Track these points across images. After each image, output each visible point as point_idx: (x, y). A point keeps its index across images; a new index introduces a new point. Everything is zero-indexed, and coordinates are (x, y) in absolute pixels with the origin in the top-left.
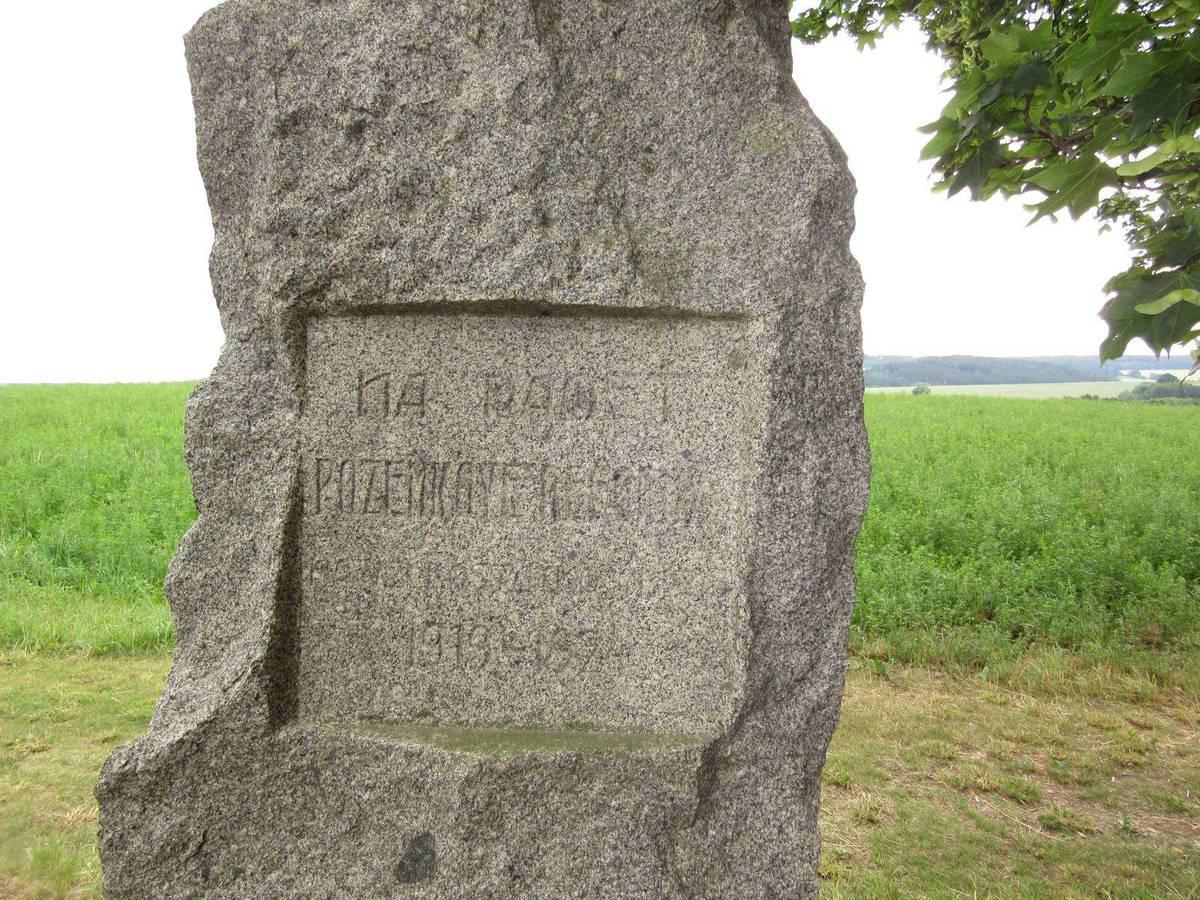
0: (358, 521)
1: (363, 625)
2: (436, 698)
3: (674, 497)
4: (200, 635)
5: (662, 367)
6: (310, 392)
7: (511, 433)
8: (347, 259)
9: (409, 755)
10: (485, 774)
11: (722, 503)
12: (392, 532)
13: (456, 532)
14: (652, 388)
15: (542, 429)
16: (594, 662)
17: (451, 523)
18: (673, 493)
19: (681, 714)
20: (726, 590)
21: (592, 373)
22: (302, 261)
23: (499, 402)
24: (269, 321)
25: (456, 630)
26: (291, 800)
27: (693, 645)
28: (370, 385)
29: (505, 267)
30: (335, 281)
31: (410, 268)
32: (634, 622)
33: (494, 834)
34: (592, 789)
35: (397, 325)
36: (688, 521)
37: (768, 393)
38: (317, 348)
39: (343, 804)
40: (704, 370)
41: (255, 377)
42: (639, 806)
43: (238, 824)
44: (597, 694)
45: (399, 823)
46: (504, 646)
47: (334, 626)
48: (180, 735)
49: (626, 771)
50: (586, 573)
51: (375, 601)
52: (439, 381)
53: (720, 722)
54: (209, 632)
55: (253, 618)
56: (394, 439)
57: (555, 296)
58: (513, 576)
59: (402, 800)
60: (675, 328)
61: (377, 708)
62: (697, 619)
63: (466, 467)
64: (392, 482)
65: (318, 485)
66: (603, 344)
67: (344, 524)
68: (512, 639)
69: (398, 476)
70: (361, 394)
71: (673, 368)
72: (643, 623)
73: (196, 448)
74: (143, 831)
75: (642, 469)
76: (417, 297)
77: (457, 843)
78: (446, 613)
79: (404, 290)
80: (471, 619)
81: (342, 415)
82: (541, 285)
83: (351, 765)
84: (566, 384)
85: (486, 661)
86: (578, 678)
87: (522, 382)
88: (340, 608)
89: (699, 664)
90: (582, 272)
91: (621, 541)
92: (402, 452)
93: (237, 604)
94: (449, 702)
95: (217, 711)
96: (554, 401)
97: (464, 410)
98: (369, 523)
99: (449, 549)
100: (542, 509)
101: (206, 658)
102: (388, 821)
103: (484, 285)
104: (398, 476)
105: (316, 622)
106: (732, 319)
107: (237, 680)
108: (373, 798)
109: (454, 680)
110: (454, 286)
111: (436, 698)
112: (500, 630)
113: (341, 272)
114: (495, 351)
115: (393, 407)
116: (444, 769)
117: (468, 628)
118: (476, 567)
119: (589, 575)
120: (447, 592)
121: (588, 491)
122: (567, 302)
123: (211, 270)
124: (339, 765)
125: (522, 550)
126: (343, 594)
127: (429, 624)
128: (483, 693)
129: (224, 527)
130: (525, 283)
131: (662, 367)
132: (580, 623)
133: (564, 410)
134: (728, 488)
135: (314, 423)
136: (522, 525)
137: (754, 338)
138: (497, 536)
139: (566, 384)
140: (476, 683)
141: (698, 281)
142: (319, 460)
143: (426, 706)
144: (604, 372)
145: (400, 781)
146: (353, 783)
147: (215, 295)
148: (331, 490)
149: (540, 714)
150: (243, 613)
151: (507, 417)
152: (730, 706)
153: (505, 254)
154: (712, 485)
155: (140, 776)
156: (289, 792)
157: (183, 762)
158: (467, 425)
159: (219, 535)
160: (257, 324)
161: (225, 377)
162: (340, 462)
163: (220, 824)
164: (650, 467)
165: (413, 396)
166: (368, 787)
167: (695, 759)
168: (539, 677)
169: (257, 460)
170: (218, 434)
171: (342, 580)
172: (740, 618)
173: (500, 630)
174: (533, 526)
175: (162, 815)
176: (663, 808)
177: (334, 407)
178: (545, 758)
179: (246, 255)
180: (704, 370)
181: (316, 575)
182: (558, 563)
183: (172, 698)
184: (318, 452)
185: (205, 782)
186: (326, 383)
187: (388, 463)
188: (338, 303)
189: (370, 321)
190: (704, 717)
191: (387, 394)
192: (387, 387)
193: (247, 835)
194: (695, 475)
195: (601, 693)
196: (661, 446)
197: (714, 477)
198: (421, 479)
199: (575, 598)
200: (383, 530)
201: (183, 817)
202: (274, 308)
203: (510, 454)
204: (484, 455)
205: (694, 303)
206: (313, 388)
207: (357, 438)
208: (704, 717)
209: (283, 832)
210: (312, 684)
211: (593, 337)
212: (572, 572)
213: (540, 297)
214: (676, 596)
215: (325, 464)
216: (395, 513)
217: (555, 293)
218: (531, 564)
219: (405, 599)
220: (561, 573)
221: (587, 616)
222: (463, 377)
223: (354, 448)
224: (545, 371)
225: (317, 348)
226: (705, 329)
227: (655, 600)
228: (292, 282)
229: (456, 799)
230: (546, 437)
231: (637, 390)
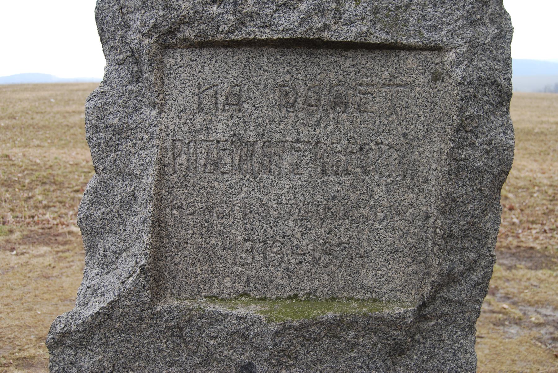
0: (200, 178)
1: (205, 242)
2: (251, 285)
3: (397, 161)
4: (102, 249)
5: (390, 80)
6: (167, 97)
7: (296, 123)
8: (192, 11)
9: (239, 319)
10: (287, 329)
11: (426, 165)
12: (221, 185)
13: (262, 184)
14: (384, 94)
15: (315, 120)
16: (347, 261)
17: (258, 179)
18: (396, 159)
19: (400, 290)
20: (427, 217)
21: (347, 84)
22: (161, 13)
23: (288, 103)
24: (139, 51)
25: (262, 244)
26: (165, 346)
27: (406, 250)
28: (205, 93)
29: (294, 17)
30: (183, 26)
31: (233, 18)
32: (371, 237)
33: (291, 362)
34: (348, 335)
35: (221, 53)
36: (405, 176)
37: (458, 97)
38: (170, 69)
39: (198, 347)
40: (417, 82)
41: (129, 88)
42: (375, 345)
43: (134, 359)
44: (349, 280)
45: (233, 358)
46: (292, 253)
47: (187, 243)
48: (97, 310)
49: (368, 324)
50: (342, 208)
51: (212, 227)
52: (249, 90)
53: (422, 295)
54: (107, 247)
55: (137, 239)
56: (221, 127)
57: (326, 35)
58: (297, 210)
59: (234, 344)
60: (398, 56)
61: (215, 291)
62: (410, 235)
63: (268, 144)
64: (221, 153)
65: (174, 156)
66: (354, 66)
67: (191, 180)
68: (297, 248)
69: (224, 150)
70: (199, 98)
71: (397, 81)
72: (377, 237)
73: (93, 133)
74: (77, 365)
75: (377, 144)
76: (236, 36)
77: (270, 368)
78: (256, 234)
79: (229, 32)
80: (272, 237)
81: (188, 112)
82: (318, 29)
83: (202, 325)
84: (330, 91)
85: (281, 262)
86: (337, 271)
87: (302, 90)
88: (190, 232)
89: (410, 261)
90: (342, 20)
91: (365, 188)
92: (226, 135)
93: (125, 230)
94: (260, 287)
95: (119, 295)
96: (323, 102)
97: (265, 108)
98: (207, 179)
99: (257, 195)
100: (315, 169)
101: (107, 263)
102: (226, 356)
103: (281, 28)
104: (224, 150)
105: (175, 240)
106: (435, 50)
107: (130, 276)
108: (216, 343)
109: (261, 274)
110: (262, 30)
111: (251, 285)
112: (290, 243)
113: (187, 20)
114: (285, 70)
115: (220, 106)
116: (261, 326)
117: (270, 242)
118: (274, 206)
119: (344, 210)
120: (257, 221)
121: (344, 158)
122: (334, 39)
123: (96, 18)
124: (195, 325)
125: (303, 195)
126: (192, 223)
127: (246, 240)
128: (280, 281)
129: (114, 182)
130: (307, 27)
131: (390, 80)
132: (339, 238)
133: (329, 108)
134: (430, 156)
135: (170, 117)
136: (303, 179)
137: (448, 62)
138: (288, 186)
139: (330, 91)
140: (276, 275)
141: (414, 26)
142: (174, 140)
143: (245, 289)
144: (354, 83)
145: (233, 333)
146: (203, 335)
147: (100, 35)
148: (182, 159)
149: (315, 292)
150: (129, 236)
151: (293, 112)
152: (429, 285)
153: (294, 8)
154: (420, 155)
155: (73, 334)
156: (164, 341)
157: (99, 326)
158: (268, 118)
159: (111, 188)
160: (129, 54)
161: (110, 88)
162: (187, 142)
163: (123, 360)
164: (382, 143)
165: (233, 99)
166: (213, 338)
167: (409, 317)
168: (314, 271)
169: (134, 141)
170: (109, 123)
171: (191, 215)
172: (436, 234)
173: (290, 243)
174: (309, 180)
175: (88, 355)
176: (389, 345)
177: (182, 107)
178: (321, 318)
179: (121, 8)
180: (417, 82)
181: (174, 212)
182: (325, 203)
183: (88, 287)
184: (173, 135)
185: (113, 336)
186: (177, 91)
187: (218, 142)
188: (185, 40)
189: (204, 51)
190: (413, 292)
191: (217, 99)
192: (216, 93)
193: (139, 366)
194: (410, 148)
195: (352, 279)
196: (389, 130)
197: (421, 149)
198: (239, 151)
199: (336, 224)
200: (216, 183)
201: (100, 357)
202: (143, 44)
203: (295, 135)
204: (278, 136)
205: (411, 40)
206: (169, 94)
207: (198, 126)
208: (413, 292)
209: (161, 363)
210: (174, 278)
211: (347, 62)
212: (334, 208)
213: (317, 36)
214: (397, 221)
215: (177, 143)
216: (223, 173)
217: (326, 33)
218: (309, 203)
219: (231, 225)
220: (327, 208)
221: (343, 232)
222: (265, 87)
223: (196, 133)
224: (317, 83)
225: (170, 69)
226: (417, 56)
227: (385, 223)
228: (155, 26)
229: (270, 344)
230: (318, 125)
231: (374, 95)
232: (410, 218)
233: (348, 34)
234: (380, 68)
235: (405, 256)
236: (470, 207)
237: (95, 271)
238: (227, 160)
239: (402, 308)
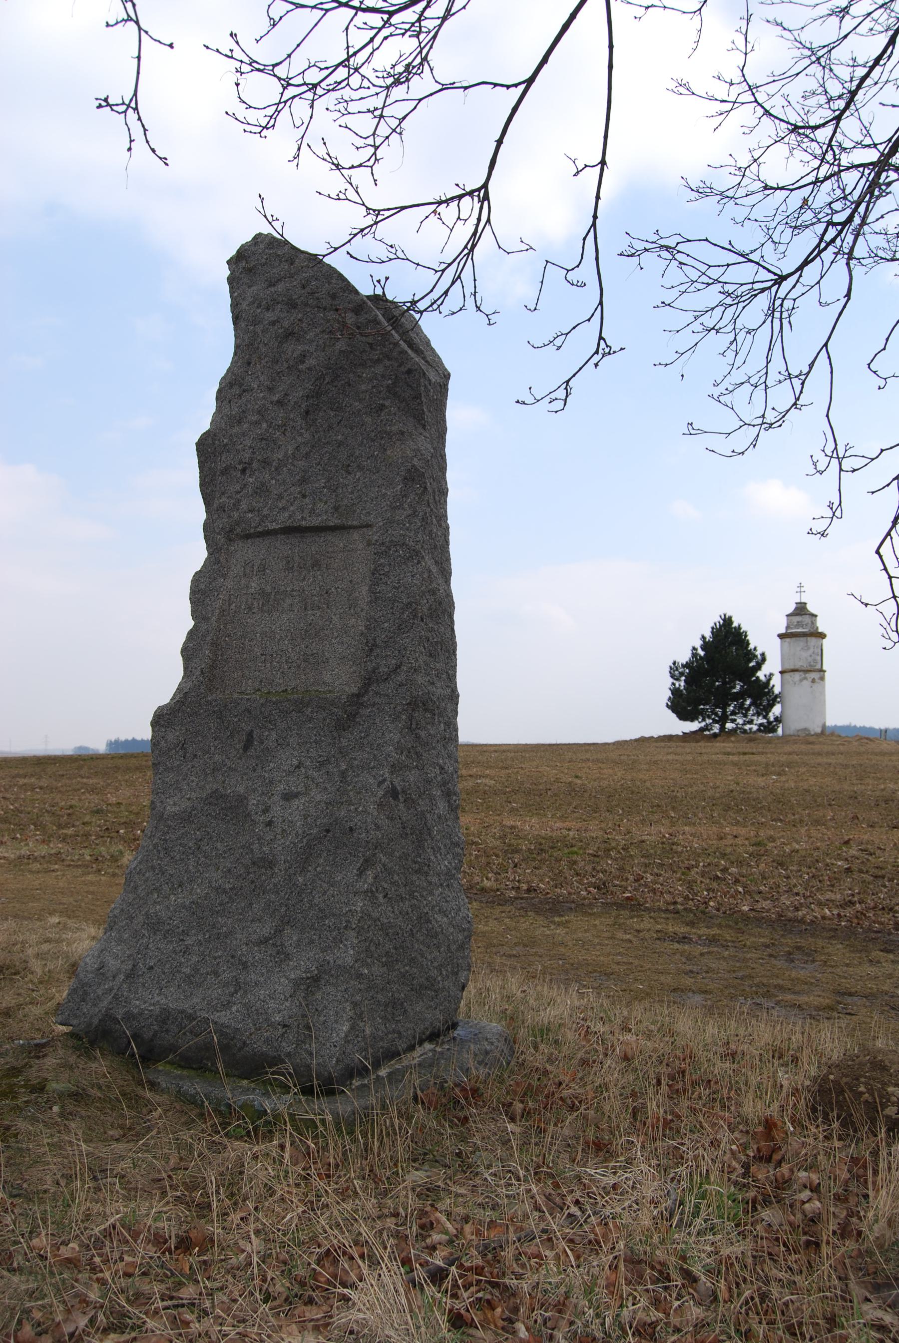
42: (324, 719)
57: (304, 523)
76: (260, 529)
87: (296, 559)
127: (262, 655)
148: (233, 606)
230: (304, 579)
232: (352, 635)
233: (316, 522)
234: (338, 541)
235: (349, 660)
236: (386, 625)
238: (256, 604)
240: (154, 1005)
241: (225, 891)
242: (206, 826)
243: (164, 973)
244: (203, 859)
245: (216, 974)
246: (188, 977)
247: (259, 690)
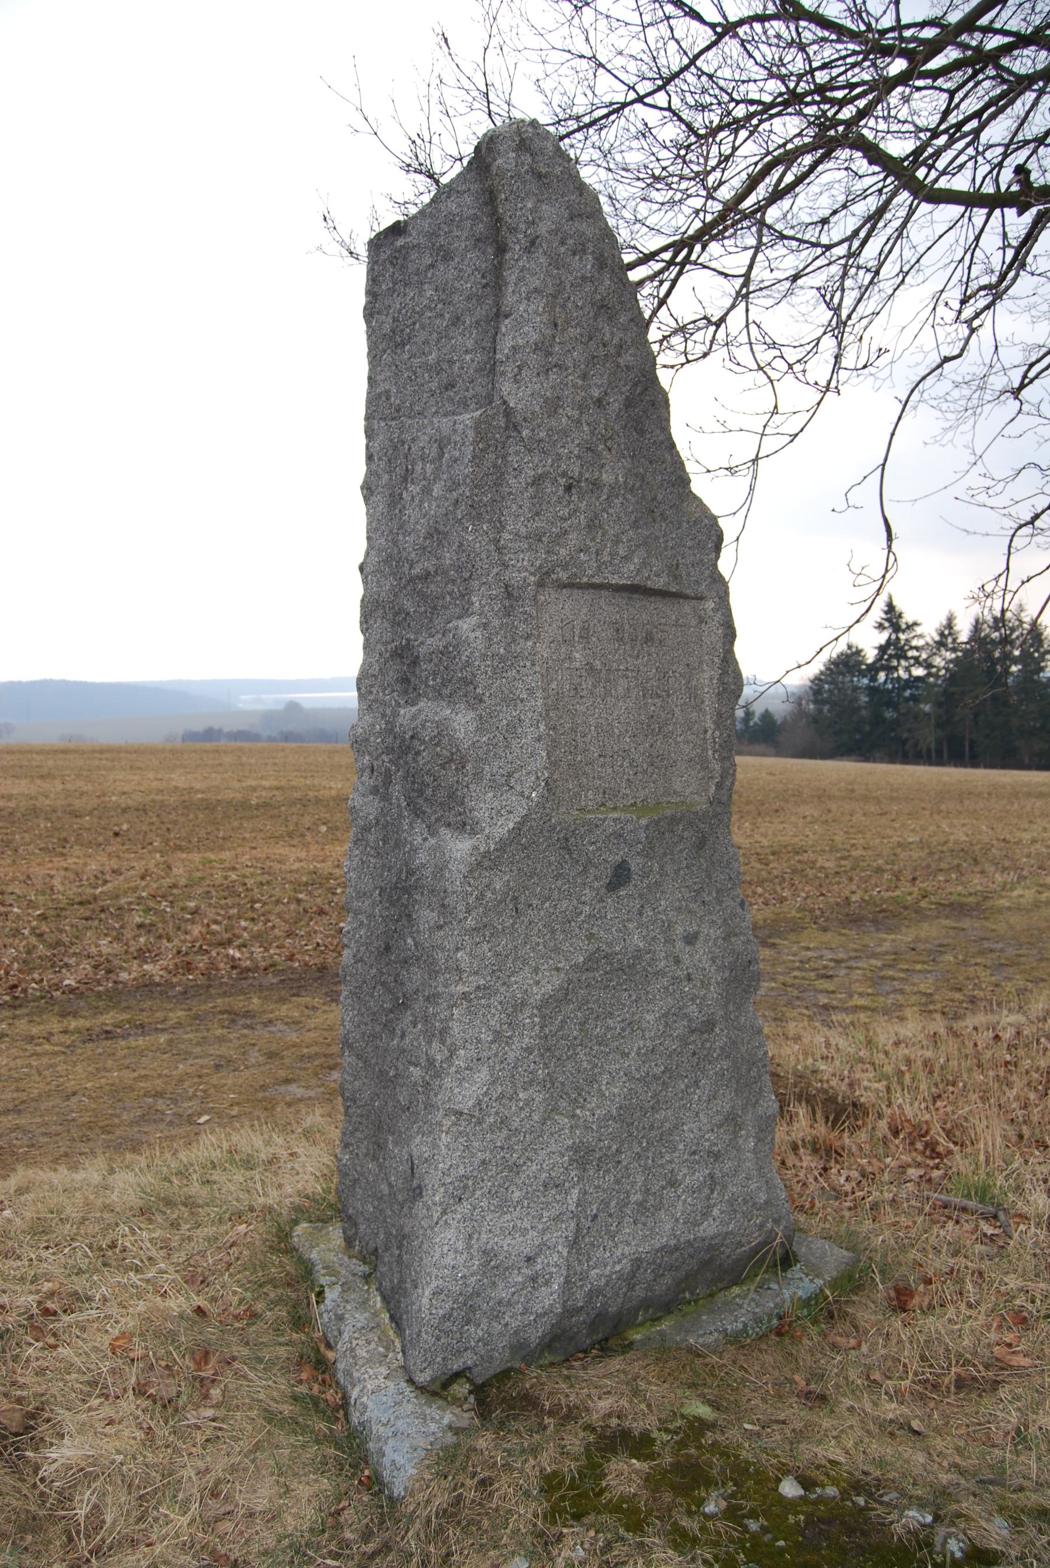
9: (615, 820)
76: (597, 580)
109: (612, 785)
228: (540, 567)
237: (491, 795)
239: (702, 805)
240: (619, 1261)
241: (656, 1078)
242: (588, 1002)
243: (610, 1215)
244: (596, 1048)
245: (673, 1184)
246: (640, 1204)
247: (603, 805)
